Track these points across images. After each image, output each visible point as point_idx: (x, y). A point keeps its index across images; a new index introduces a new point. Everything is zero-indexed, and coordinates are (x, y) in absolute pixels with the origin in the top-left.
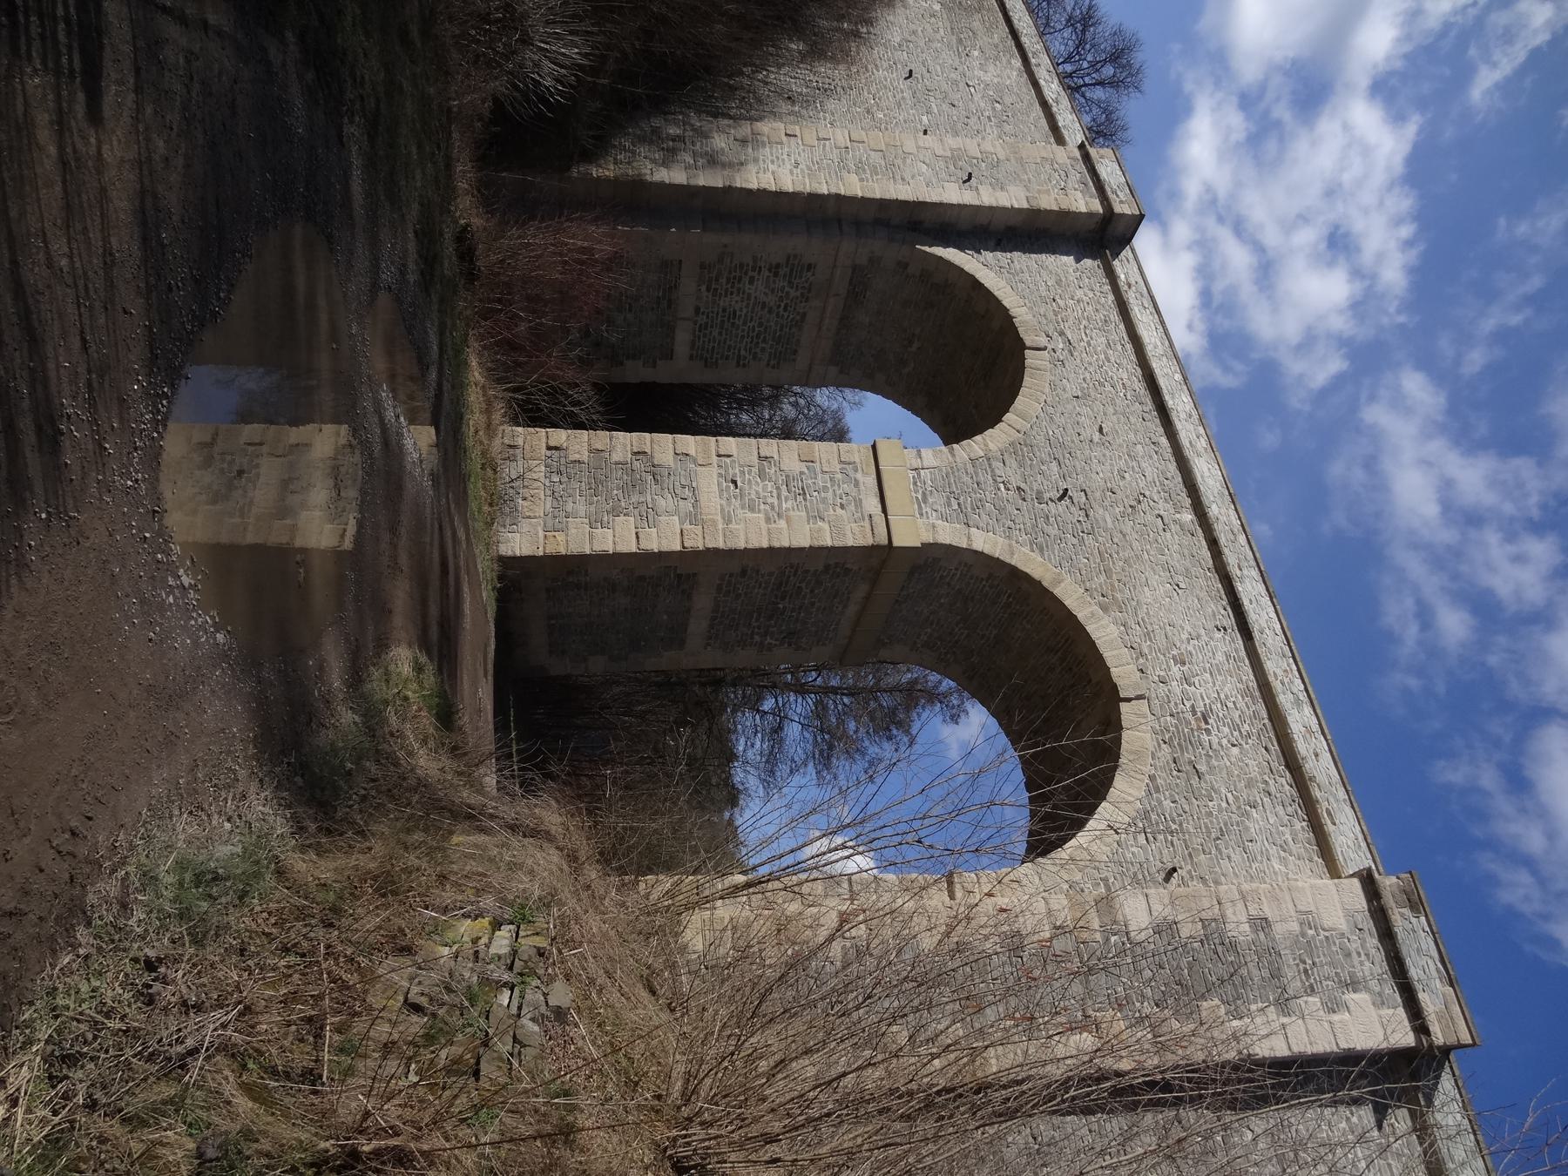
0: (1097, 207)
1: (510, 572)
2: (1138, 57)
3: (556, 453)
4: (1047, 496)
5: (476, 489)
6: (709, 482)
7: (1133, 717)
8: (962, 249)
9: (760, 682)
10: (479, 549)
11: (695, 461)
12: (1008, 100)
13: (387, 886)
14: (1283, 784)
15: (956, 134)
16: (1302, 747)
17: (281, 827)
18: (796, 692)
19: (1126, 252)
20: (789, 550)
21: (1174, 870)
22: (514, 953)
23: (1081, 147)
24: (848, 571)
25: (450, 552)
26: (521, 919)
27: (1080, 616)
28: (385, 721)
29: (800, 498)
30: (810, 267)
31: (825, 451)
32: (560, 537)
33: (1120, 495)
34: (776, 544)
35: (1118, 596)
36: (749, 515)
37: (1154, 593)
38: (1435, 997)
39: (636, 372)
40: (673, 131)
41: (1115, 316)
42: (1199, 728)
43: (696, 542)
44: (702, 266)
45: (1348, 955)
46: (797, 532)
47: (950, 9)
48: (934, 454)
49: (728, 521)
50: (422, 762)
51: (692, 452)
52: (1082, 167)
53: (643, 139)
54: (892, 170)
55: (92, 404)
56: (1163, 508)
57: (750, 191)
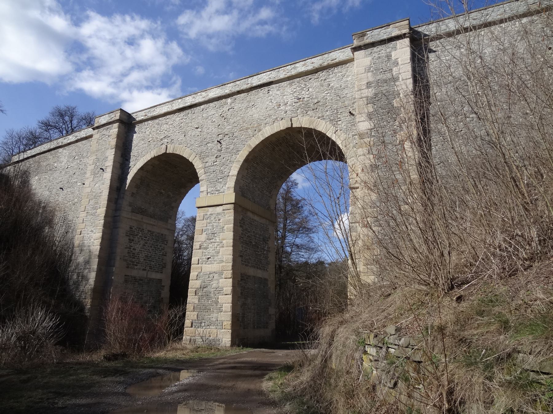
0: (116, 125)
2: (62, 107)
3: (194, 324)
4: (219, 148)
5: (205, 355)
6: (208, 268)
8: (129, 173)
9: (280, 252)
12: (74, 154)
13: (350, 394)
14: (322, 75)
15: (85, 173)
16: (310, 68)
20: (234, 239)
21: (350, 112)
22: (376, 346)
23: (94, 129)
24: (243, 219)
27: (262, 139)
28: (289, 393)
30: (130, 228)
32: (225, 323)
34: (232, 244)
35: (256, 125)
36: (220, 253)
37: (255, 114)
39: (166, 293)
40: (75, 277)
41: (157, 121)
42: (302, 101)
43: (229, 273)
44: (128, 267)
47: (38, 173)
48: (202, 186)
51: (196, 273)
53: (77, 288)
56: (226, 108)
57: (101, 249)
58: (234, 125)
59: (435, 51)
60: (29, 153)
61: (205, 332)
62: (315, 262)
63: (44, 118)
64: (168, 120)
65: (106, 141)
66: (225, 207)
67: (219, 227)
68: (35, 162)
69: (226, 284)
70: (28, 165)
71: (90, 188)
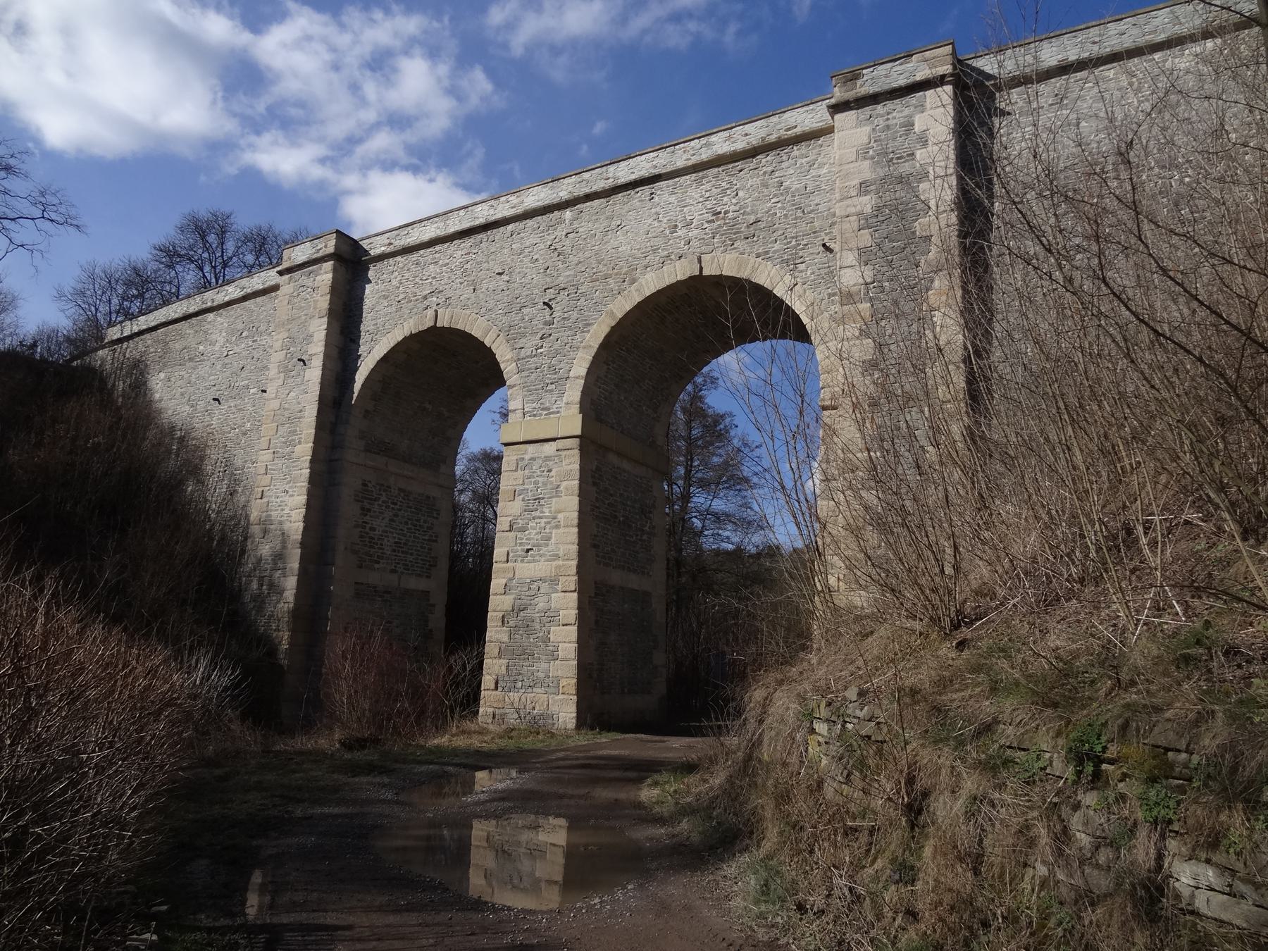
0: (329, 265)
1: (589, 721)
2: (203, 214)
3: (500, 684)
4: (548, 318)
5: (528, 743)
6: (527, 570)
7: (715, 265)
8: (357, 369)
9: (680, 529)
10: (571, 743)
11: (511, 580)
12: (240, 326)
13: (783, 798)
14: (766, 161)
15: (266, 368)
16: (740, 145)
17: (746, 858)
18: (688, 502)
19: (364, 244)
20: (580, 512)
21: (824, 245)
22: (827, 720)
23: (281, 273)
24: (598, 469)
25: (575, 762)
26: (810, 716)
27: (639, 300)
28: (689, 804)
29: (542, 502)
30: (365, 485)
31: (507, 481)
32: (563, 683)
33: (549, 263)
34: (576, 522)
35: (624, 270)
36: (553, 540)
37: (624, 244)
38: (917, 69)
39: (438, 620)
40: (255, 585)
41: (413, 257)
42: (724, 218)
43: (571, 581)
44: (360, 567)
45: (888, 127)
46: (567, 505)
47: (165, 365)
48: (513, 396)
49: (557, 557)
50: (717, 781)
51: (504, 581)
52: (297, 274)
53: (260, 609)
54: (294, 419)
55: (506, 933)
56: (561, 232)
57: (305, 528)
58: (578, 269)
59: (1009, 114)
60: (143, 322)
61: (523, 699)
62: (753, 550)
63: (163, 240)
64: (437, 255)
65: (308, 300)
66: (560, 444)
67: (549, 487)
68: (157, 341)
69: (565, 604)
70: (141, 347)
71: (278, 401)
